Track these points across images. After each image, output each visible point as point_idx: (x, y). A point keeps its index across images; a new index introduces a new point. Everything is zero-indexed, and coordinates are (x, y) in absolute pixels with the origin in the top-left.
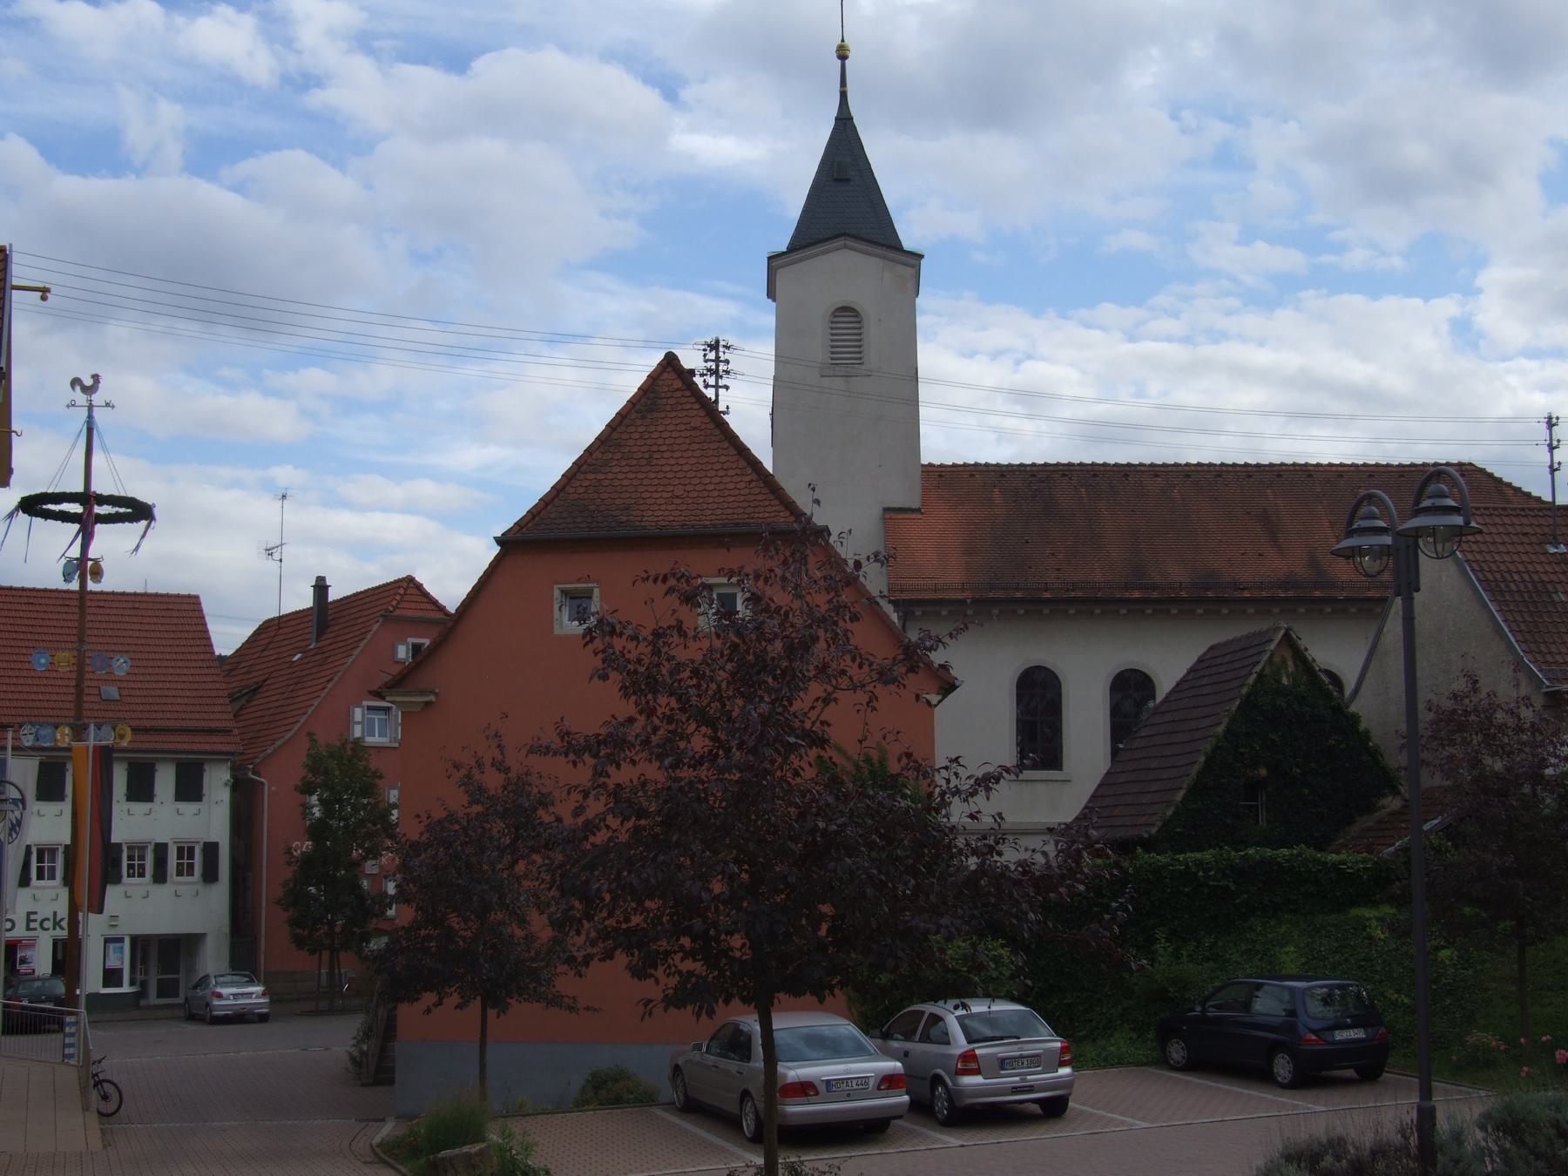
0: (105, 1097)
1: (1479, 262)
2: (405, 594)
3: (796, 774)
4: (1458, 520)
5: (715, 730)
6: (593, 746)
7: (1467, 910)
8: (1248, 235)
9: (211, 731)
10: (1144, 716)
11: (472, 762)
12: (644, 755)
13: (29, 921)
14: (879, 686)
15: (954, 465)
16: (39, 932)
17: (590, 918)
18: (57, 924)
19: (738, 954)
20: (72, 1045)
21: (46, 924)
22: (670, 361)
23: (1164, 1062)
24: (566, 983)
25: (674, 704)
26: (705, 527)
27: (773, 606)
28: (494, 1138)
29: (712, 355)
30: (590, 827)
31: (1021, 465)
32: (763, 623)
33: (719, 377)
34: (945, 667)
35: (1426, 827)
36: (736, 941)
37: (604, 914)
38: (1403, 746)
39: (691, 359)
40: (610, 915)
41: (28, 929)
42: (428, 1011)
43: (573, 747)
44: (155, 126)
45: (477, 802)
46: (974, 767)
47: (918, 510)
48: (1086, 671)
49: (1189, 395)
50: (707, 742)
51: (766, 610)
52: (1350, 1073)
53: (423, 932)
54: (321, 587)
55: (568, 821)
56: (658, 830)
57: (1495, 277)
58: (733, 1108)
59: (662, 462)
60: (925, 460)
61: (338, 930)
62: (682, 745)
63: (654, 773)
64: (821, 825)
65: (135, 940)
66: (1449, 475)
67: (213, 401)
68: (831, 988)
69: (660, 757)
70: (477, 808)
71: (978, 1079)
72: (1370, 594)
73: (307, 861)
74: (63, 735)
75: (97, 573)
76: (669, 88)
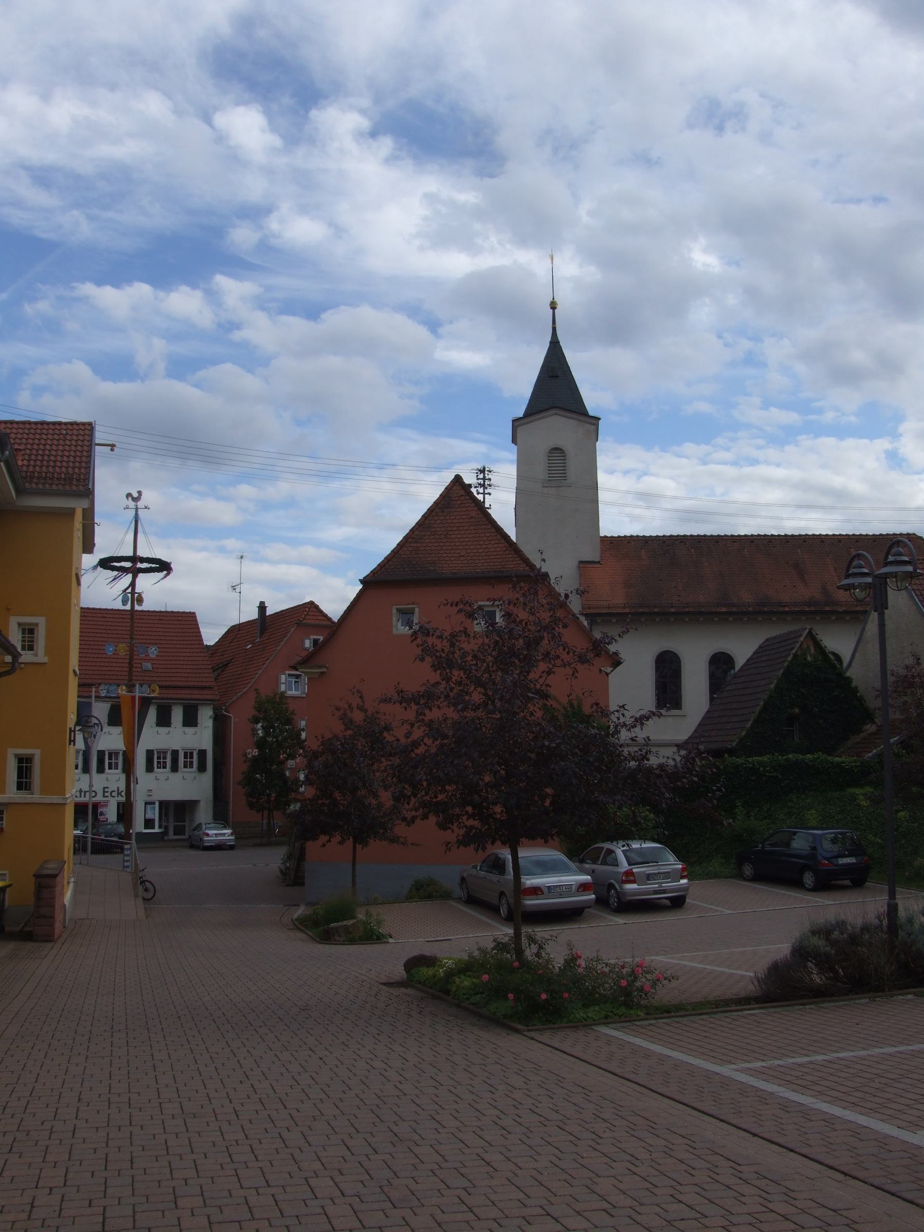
0: (146, 890)
1: (899, 418)
2: (308, 613)
3: (532, 714)
4: (910, 568)
5: (486, 689)
6: (415, 699)
7: (914, 789)
8: (766, 404)
9: (203, 688)
10: (728, 679)
11: (346, 706)
12: (446, 703)
13: (104, 792)
14: (579, 665)
15: (619, 537)
16: (110, 798)
17: (415, 796)
18: (119, 794)
19: (499, 816)
20: (128, 861)
21: (114, 794)
22: (458, 479)
23: (740, 876)
24: (400, 829)
25: (462, 674)
26: (478, 573)
27: (518, 620)
28: (361, 916)
29: (481, 476)
30: (415, 744)
31: (657, 536)
32: (513, 629)
33: (485, 488)
34: (616, 654)
35: (892, 741)
36: (498, 809)
37: (423, 793)
38: (877, 696)
39: (469, 478)
40: (426, 794)
41: (104, 796)
42: (324, 845)
43: (404, 699)
44: (151, 351)
45: (349, 729)
46: (633, 711)
47: (599, 562)
48: (695, 654)
49: (741, 495)
50: (481, 696)
51: (514, 622)
52: (847, 882)
53: (320, 802)
54: (262, 607)
55: (403, 740)
56: (453, 746)
57: (908, 427)
58: (496, 902)
59: (453, 536)
60: (602, 534)
61: (272, 799)
62: (467, 698)
63: (452, 713)
64: (546, 743)
65: (162, 803)
66: (902, 542)
67: (195, 503)
68: (552, 836)
69: (455, 705)
70: (350, 732)
71: (635, 886)
72: (858, 609)
73: (255, 760)
74: (122, 690)
75: (140, 600)
76: (434, 326)
